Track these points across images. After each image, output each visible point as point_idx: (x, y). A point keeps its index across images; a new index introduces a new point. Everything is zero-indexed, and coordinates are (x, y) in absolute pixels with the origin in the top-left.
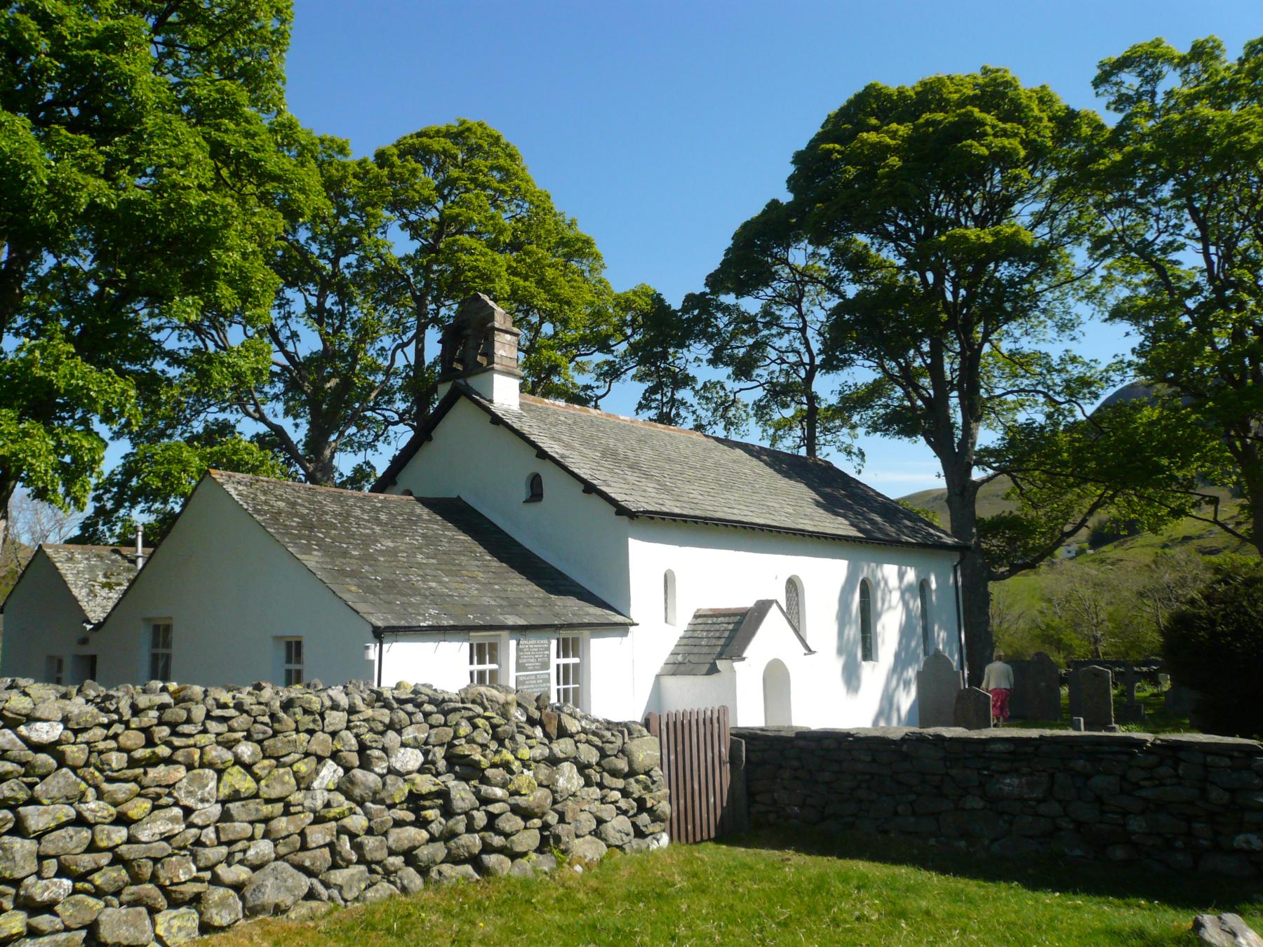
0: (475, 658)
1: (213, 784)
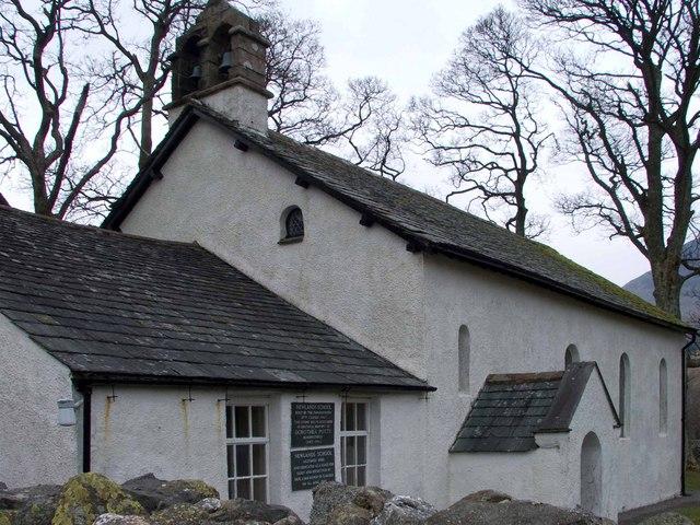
0: (234, 433)
1: (299, 61)
